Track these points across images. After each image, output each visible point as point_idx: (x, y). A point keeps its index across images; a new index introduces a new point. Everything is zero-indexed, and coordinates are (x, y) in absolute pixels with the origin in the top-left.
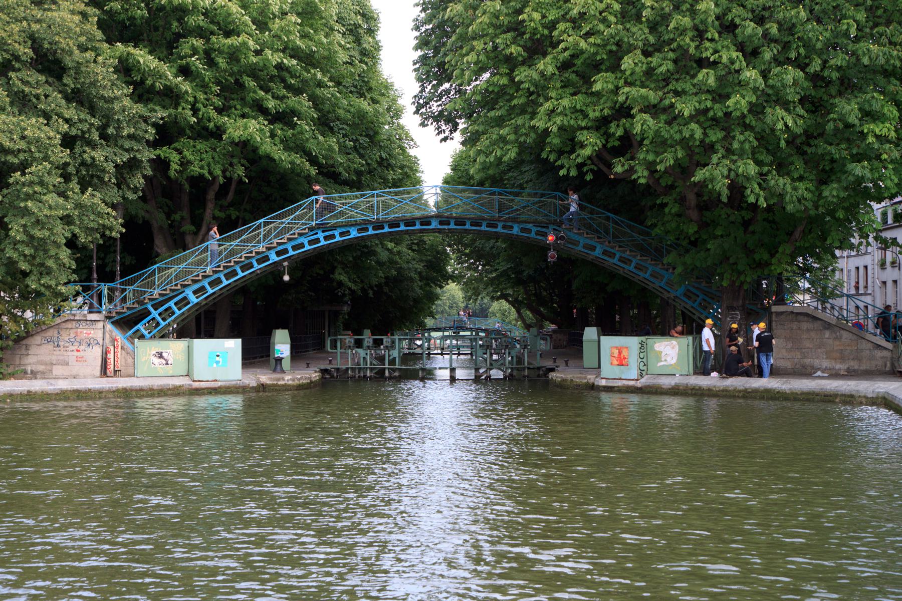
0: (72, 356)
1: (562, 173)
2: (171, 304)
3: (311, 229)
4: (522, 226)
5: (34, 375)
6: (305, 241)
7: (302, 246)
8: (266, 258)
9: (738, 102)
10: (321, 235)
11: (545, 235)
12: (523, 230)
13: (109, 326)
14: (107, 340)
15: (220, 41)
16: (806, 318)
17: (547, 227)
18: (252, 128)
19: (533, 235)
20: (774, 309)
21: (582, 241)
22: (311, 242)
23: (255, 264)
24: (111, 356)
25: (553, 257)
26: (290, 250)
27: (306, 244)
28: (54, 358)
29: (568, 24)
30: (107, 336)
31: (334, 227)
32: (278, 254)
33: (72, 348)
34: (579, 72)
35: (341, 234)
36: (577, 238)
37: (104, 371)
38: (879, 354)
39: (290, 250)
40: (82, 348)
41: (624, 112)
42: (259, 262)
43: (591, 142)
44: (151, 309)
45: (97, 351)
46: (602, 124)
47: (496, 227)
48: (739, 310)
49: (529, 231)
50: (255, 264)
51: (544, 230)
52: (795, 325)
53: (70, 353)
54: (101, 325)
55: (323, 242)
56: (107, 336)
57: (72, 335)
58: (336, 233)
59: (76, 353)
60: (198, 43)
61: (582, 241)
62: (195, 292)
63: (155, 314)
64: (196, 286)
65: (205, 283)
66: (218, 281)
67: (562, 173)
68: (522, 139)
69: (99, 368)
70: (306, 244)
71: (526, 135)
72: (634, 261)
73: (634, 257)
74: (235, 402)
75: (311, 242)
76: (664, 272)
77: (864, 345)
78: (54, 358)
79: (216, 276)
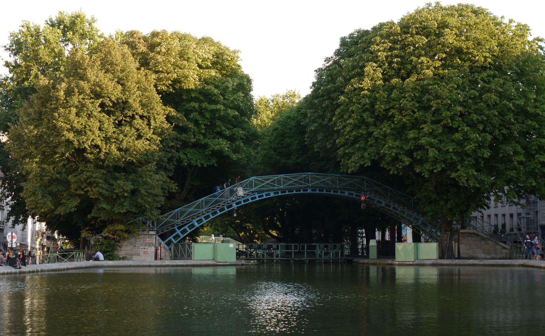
0: (142, 251)
1: (391, 173)
2: (186, 227)
3: (253, 192)
4: (350, 192)
5: (124, 258)
6: (249, 198)
7: (248, 200)
8: (231, 206)
9: (470, 147)
11: (359, 196)
12: (350, 194)
13: (158, 237)
14: (157, 244)
15: (205, 105)
18: (224, 145)
19: (354, 196)
20: (461, 231)
21: (377, 199)
22: (252, 199)
23: (226, 209)
24: (159, 251)
25: (364, 206)
26: (242, 202)
27: (250, 199)
28: (133, 252)
29: (523, 170)
30: (157, 242)
31: (263, 192)
32: (237, 204)
33: (141, 247)
34: (400, 132)
35: (266, 195)
36: (374, 198)
37: (156, 258)
38: (504, 251)
39: (242, 202)
40: (146, 247)
41: (420, 147)
42: (228, 207)
43: (407, 161)
44: (177, 230)
45: (153, 249)
46: (409, 153)
47: (337, 192)
49: (352, 194)
50: (226, 209)
52: (470, 239)
53: (140, 250)
54: (154, 237)
55: (258, 199)
56: (157, 242)
57: (142, 241)
58: (264, 194)
59: (143, 250)
60: (196, 105)
61: (377, 199)
62: (197, 222)
63: (179, 232)
64: (198, 219)
65: (202, 217)
66: (208, 217)
67: (391, 173)
68: (373, 158)
69: (154, 257)
70: (250, 199)
71: (375, 156)
72: (399, 209)
73: (399, 207)
74: (232, 271)
75: (252, 199)
76: (412, 214)
77: (498, 247)
78: (133, 252)
79: (208, 214)
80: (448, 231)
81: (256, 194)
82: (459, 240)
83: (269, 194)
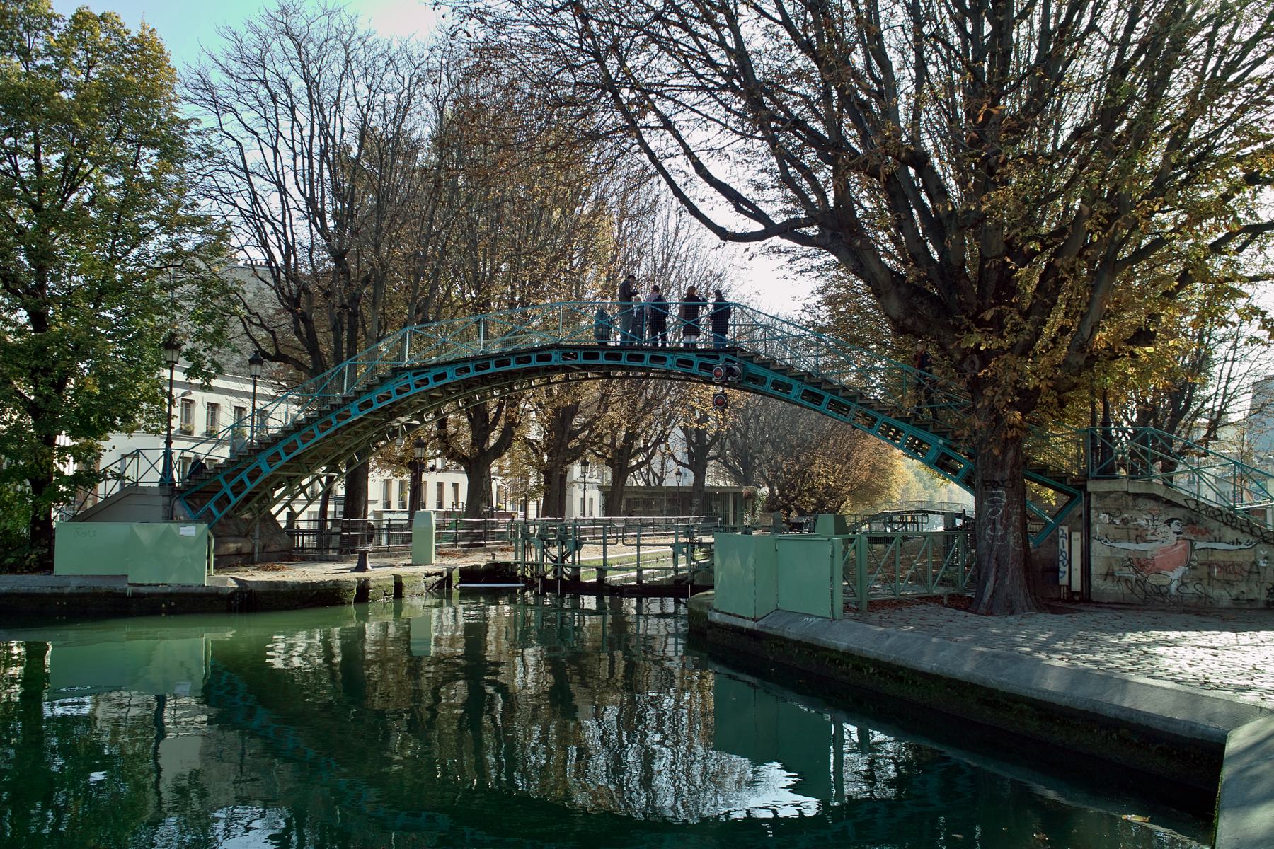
10: (412, 381)
16: (1151, 504)
17: (717, 358)
48: (1005, 488)
51: (710, 361)
58: (430, 376)
80: (995, 485)
81: (409, 374)
82: (1088, 525)
83: (444, 376)
